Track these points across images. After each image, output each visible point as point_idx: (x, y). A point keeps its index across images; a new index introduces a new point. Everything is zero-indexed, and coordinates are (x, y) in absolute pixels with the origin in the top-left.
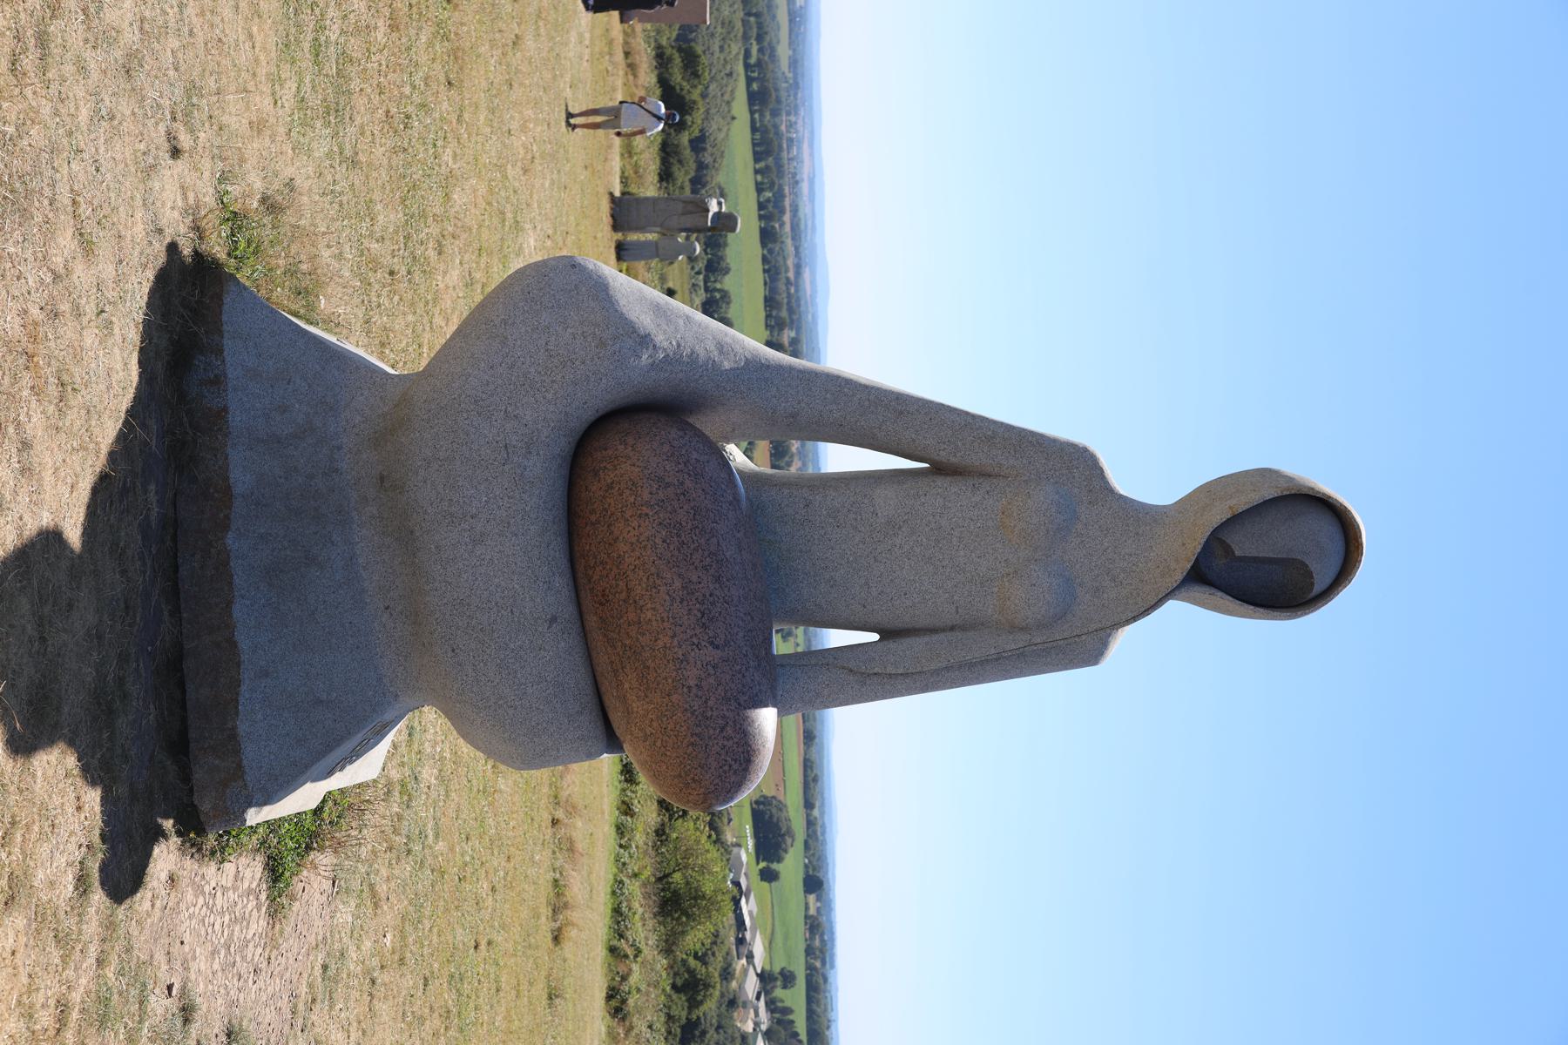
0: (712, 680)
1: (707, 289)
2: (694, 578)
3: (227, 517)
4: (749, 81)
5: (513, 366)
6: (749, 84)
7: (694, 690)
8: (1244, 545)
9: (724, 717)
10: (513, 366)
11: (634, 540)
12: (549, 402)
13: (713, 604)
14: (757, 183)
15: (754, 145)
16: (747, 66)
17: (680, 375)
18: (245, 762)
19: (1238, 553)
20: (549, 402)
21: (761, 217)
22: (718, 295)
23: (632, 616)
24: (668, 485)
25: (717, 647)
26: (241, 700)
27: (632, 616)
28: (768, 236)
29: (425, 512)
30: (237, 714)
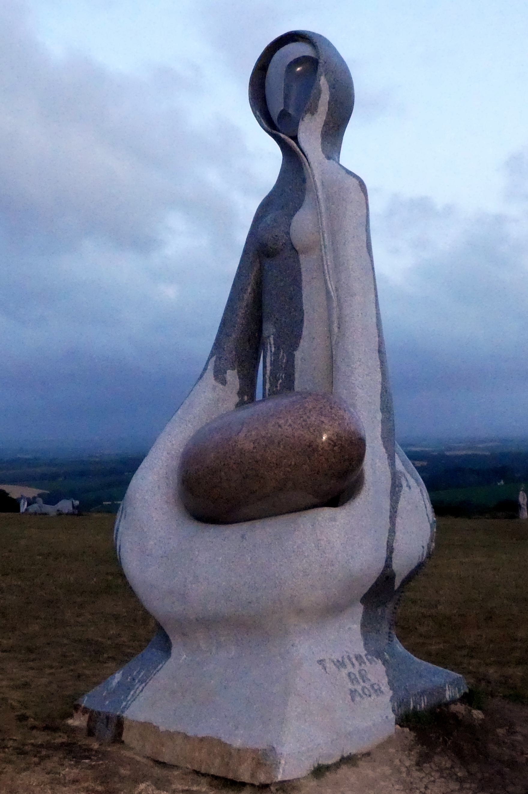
0: (253, 433)
3: (154, 727)
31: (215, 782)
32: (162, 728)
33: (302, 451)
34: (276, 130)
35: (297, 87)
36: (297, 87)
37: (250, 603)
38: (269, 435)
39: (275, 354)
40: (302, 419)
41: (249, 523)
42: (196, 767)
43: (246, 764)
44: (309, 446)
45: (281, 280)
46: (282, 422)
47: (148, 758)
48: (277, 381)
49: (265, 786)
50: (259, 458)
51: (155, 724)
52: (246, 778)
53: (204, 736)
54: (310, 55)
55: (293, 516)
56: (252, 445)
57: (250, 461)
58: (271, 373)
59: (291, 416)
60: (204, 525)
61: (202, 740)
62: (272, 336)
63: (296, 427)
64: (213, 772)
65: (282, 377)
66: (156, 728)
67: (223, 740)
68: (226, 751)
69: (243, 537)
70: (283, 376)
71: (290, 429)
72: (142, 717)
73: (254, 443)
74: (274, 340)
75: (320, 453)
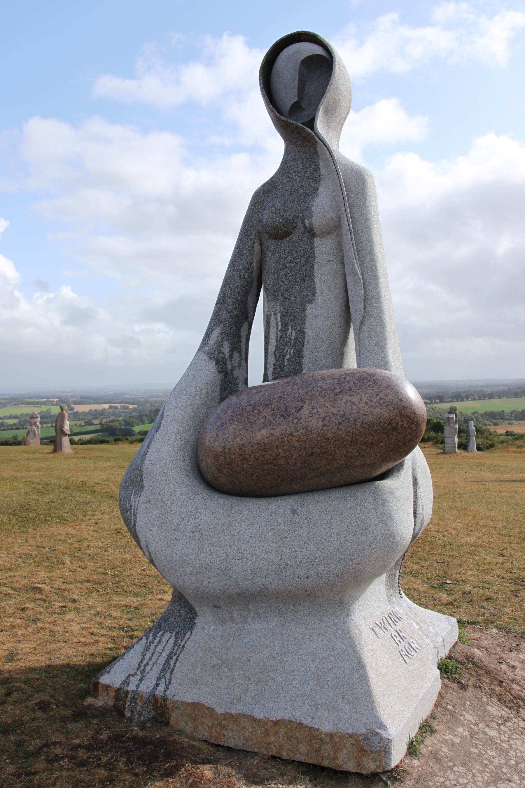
0: (321, 411)
1: (510, 419)
2: (262, 421)
3: (208, 708)
4: (435, 403)
5: (152, 524)
6: (437, 403)
7: (326, 422)
8: (288, 96)
9: (346, 403)
10: (152, 524)
11: (241, 458)
12: (172, 504)
13: (278, 409)
14: (472, 400)
15: (458, 401)
16: (431, 403)
17: (177, 426)
18: (350, 731)
19: (296, 99)
20: (172, 504)
21: (484, 399)
22: (513, 415)
23: (283, 462)
24: (217, 436)
25: (302, 406)
26: (311, 725)
27: (283, 462)
28: (491, 396)
29: (226, 585)
30: (318, 730)
31: (302, 769)
32: (219, 711)
33: (382, 429)
34: (282, 120)
35: (299, 81)
36: (299, 81)
37: (308, 578)
38: (342, 413)
39: (282, 330)
40: (378, 397)
41: (296, 497)
42: (274, 752)
43: (345, 751)
44: (388, 424)
45: (291, 262)
46: (355, 399)
47: (203, 741)
48: (284, 356)
49: (375, 776)
50: (330, 435)
51: (208, 705)
52: (350, 766)
53: (278, 719)
54: (320, 53)
55: (348, 492)
56: (320, 424)
57: (319, 438)
58: (277, 348)
59: (365, 394)
60: (241, 498)
61: (277, 723)
62: (279, 314)
63: (373, 404)
64: (298, 758)
65: (290, 352)
66: (211, 710)
67: (305, 722)
68: (312, 735)
69: (294, 511)
70: (292, 352)
71: (367, 408)
72: (188, 697)
73: (323, 421)
74: (281, 317)
75: (398, 431)
